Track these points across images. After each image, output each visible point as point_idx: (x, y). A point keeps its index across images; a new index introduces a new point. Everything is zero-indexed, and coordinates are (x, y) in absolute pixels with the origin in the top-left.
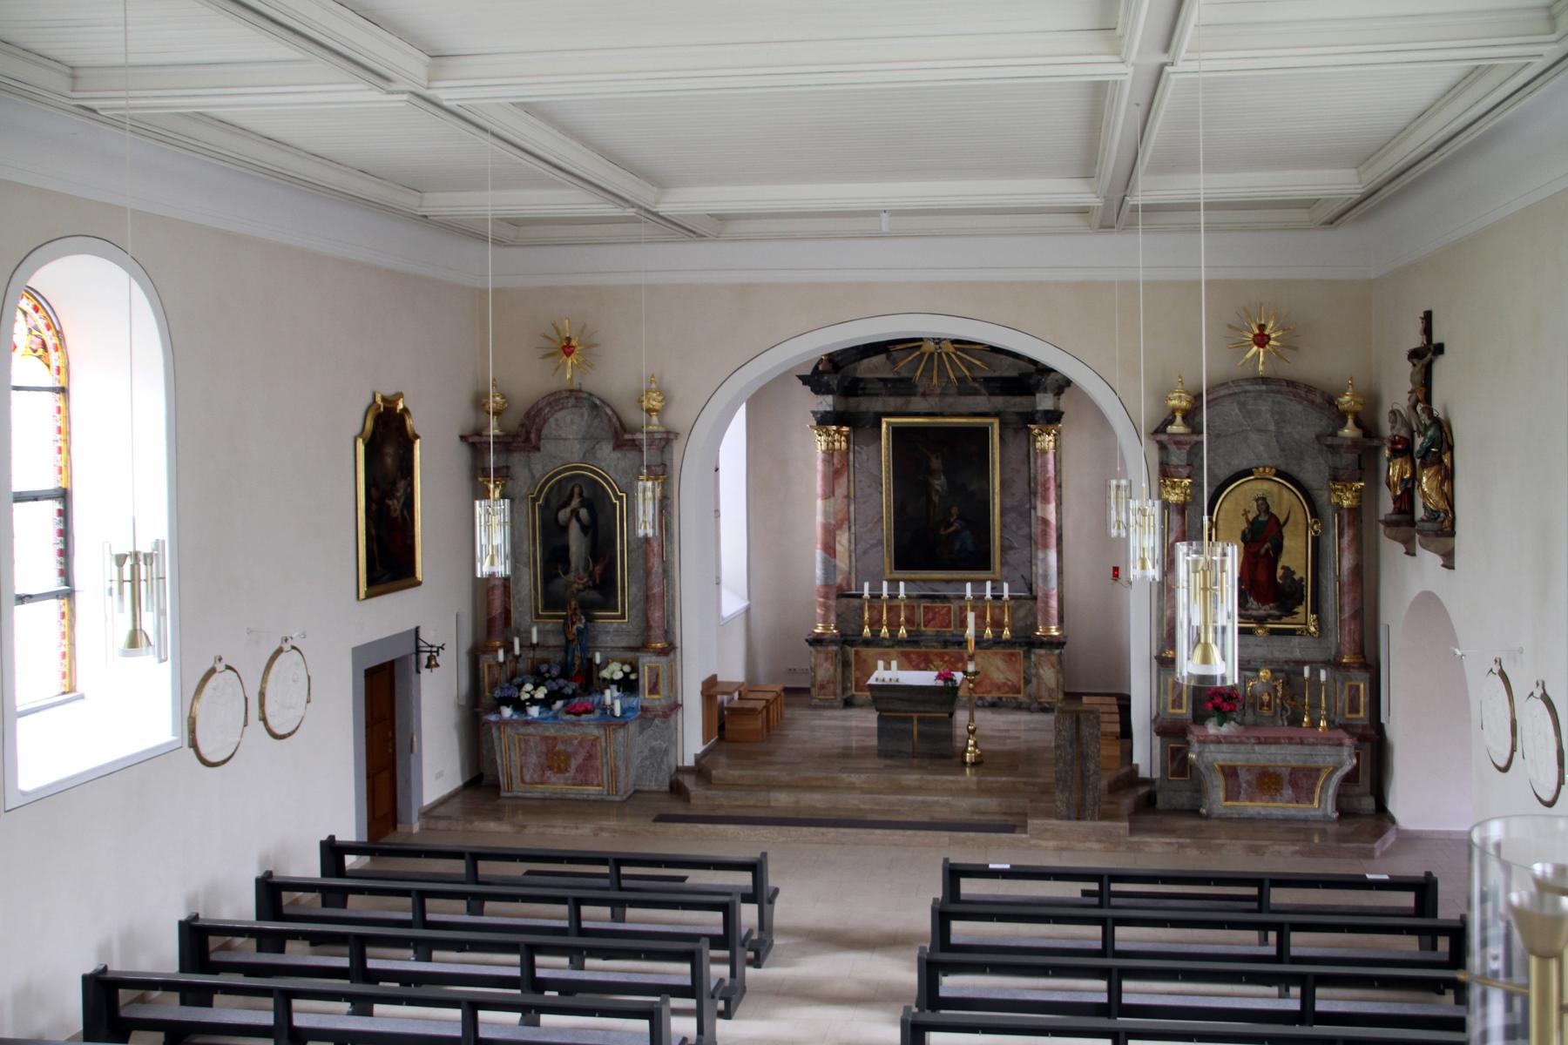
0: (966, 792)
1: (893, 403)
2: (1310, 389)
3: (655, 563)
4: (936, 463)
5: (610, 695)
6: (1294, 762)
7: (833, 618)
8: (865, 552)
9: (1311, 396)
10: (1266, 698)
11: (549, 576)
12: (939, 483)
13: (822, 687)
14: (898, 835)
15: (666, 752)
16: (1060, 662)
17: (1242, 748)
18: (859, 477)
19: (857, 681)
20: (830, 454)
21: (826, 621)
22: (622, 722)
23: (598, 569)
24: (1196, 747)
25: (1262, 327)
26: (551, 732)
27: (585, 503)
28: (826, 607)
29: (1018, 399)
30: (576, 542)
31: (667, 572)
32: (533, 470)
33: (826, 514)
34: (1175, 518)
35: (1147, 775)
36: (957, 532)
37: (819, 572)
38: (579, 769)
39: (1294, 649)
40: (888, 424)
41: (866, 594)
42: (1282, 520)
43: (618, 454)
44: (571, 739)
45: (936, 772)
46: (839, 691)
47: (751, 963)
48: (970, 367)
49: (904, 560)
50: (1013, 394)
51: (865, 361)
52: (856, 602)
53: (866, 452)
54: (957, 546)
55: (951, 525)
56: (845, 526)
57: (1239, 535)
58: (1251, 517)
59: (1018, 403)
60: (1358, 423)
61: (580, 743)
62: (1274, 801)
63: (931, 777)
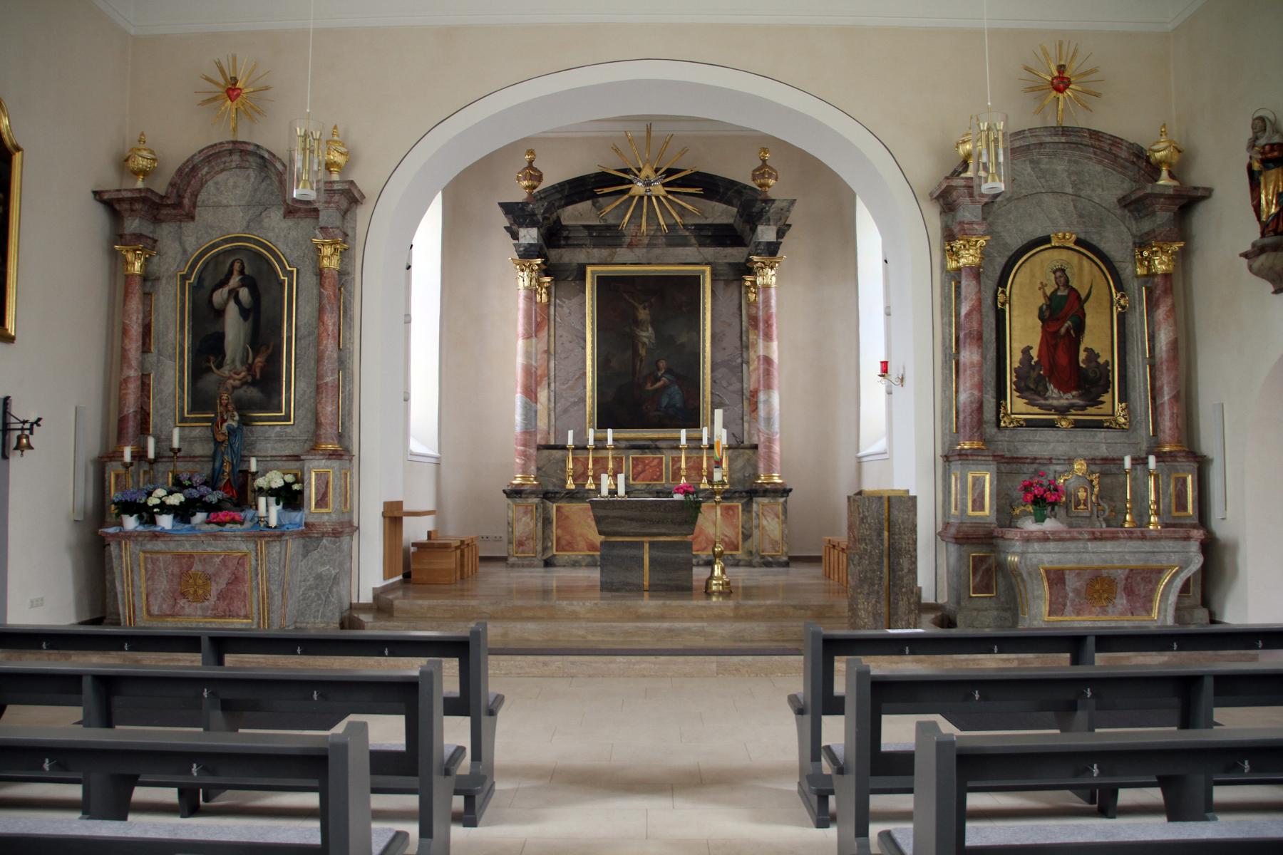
0: (721, 618)
1: (599, 253)
2: (1116, 141)
3: (329, 345)
4: (643, 314)
5: (270, 511)
6: (1133, 562)
8: (565, 411)
9: (1115, 150)
10: (1082, 494)
11: (198, 372)
13: (521, 544)
14: (646, 663)
15: (336, 580)
16: (785, 511)
17: (1072, 546)
18: (559, 332)
19: (558, 539)
20: (531, 293)
21: (525, 471)
22: (279, 534)
23: (260, 360)
24: (1018, 546)
25: (1061, 68)
26: (187, 548)
27: (248, 281)
28: (525, 455)
29: (729, 250)
30: (234, 328)
31: (343, 363)
32: (180, 248)
33: (528, 354)
34: (968, 285)
35: (933, 601)
36: (665, 387)
37: (518, 418)
38: (221, 596)
39: (1101, 444)
40: (593, 272)
41: (570, 442)
42: (1083, 296)
43: (289, 222)
44: (211, 556)
46: (539, 548)
47: (459, 819)
48: (682, 212)
49: (605, 419)
51: (570, 208)
52: (558, 454)
53: (568, 306)
54: (665, 401)
55: (658, 379)
56: (545, 383)
57: (1036, 313)
58: (1049, 291)
59: (735, 254)
60: (1171, 176)
61: (223, 561)
62: (1105, 612)
63: (675, 603)
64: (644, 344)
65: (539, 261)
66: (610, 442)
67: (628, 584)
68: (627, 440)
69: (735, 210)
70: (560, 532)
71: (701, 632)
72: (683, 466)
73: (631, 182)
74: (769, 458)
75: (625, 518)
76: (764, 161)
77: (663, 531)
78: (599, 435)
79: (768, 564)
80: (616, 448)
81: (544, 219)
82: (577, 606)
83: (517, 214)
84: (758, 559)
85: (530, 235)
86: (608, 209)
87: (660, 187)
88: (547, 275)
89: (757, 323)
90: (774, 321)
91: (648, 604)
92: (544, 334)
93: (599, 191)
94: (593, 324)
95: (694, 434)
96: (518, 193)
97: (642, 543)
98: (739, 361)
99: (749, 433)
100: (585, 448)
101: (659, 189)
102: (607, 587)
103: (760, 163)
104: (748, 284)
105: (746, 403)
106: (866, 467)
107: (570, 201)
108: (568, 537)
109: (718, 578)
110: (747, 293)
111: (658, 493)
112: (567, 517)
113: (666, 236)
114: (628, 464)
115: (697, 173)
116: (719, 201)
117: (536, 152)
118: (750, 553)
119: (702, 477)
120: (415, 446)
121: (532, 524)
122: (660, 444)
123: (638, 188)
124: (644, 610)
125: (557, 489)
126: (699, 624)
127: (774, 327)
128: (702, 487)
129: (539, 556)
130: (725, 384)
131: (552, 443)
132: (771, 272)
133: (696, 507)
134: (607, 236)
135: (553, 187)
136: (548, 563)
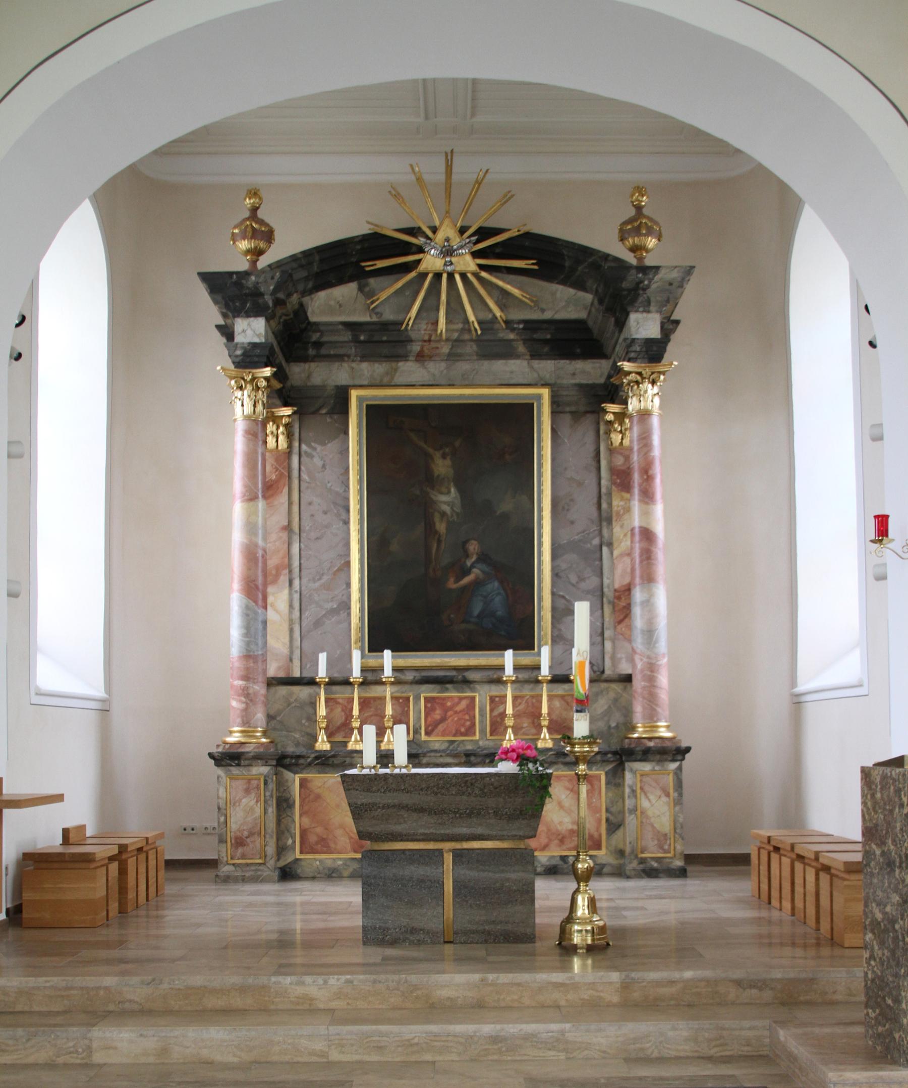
0: (593, 1008)
1: (367, 369)
4: (442, 466)
7: (260, 717)
8: (318, 624)
12: (447, 500)
13: (239, 842)
16: (679, 785)
18: (306, 498)
19: (304, 833)
20: (256, 431)
21: (246, 721)
28: (247, 695)
29: (579, 365)
33: (250, 528)
37: (235, 633)
40: (360, 399)
45: (509, 968)
46: (271, 850)
48: (504, 298)
50: (570, 355)
51: (322, 294)
52: (303, 692)
53: (320, 454)
55: (466, 572)
56: (284, 579)
59: (591, 371)
63: (504, 978)
64: (443, 514)
65: (267, 371)
66: (388, 672)
67: (413, 931)
68: (417, 669)
69: (589, 297)
70: (306, 821)
71: (558, 1043)
72: (509, 710)
73: (420, 250)
74: (651, 698)
75: (407, 808)
76: (639, 208)
77: (479, 831)
78: (372, 662)
79: (650, 873)
80: (397, 682)
81: (278, 302)
82: (317, 988)
83: (231, 293)
84: (635, 864)
85: (252, 330)
86: (384, 296)
87: (468, 258)
88: (286, 405)
89: (628, 477)
90: (657, 471)
91: (454, 981)
92: (283, 499)
93: (369, 266)
94: (360, 482)
95: (526, 659)
96: (234, 257)
97: (440, 851)
98: (596, 541)
99: (613, 658)
100: (347, 683)
101: (466, 263)
102: (374, 936)
103: (632, 212)
104: (610, 417)
105: (617, 608)
106: (812, 713)
107: (323, 282)
108: (319, 830)
109: (584, 921)
110: (608, 433)
111: (469, 758)
112: (318, 797)
113: (478, 341)
114: (417, 710)
115: (528, 235)
116: (563, 282)
117: (262, 193)
118: (621, 853)
119: (539, 728)
120: (49, 676)
121: (258, 810)
122: (471, 676)
123: (432, 261)
124: (445, 993)
125: (300, 751)
126: (554, 1027)
127: (658, 480)
128: (540, 745)
129: (271, 863)
130: (573, 578)
131: (297, 674)
132: (651, 390)
133: (540, 787)
134: (383, 341)
135: (294, 258)
136: (287, 874)
